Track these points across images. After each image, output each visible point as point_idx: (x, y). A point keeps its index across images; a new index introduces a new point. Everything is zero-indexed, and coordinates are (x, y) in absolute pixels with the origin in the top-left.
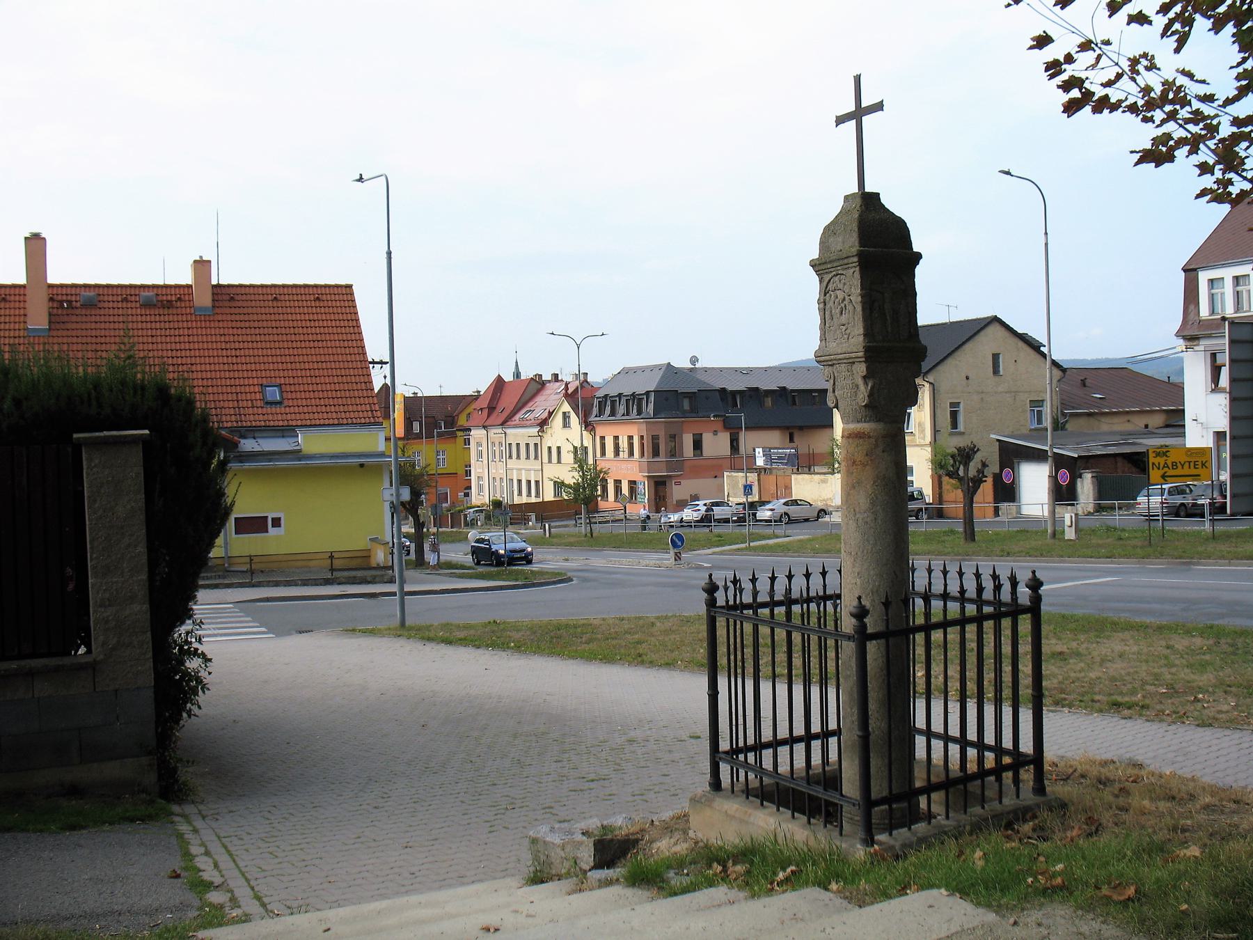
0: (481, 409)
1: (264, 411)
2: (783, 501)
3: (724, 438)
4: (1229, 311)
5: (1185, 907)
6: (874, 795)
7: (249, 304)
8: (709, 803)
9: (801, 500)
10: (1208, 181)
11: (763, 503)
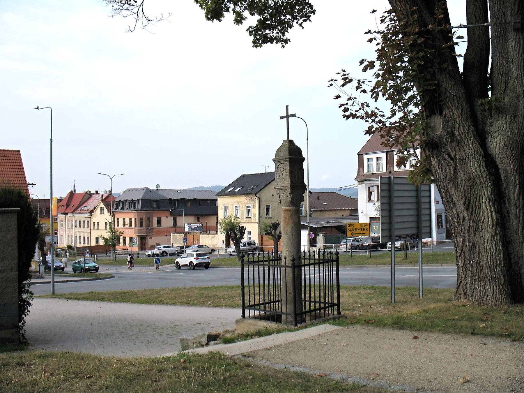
0: (63, 206)
2: (197, 245)
3: (170, 219)
4: (375, 171)
5: (386, 322)
6: (297, 312)
8: (243, 321)
9: (204, 245)
10: (383, 140)
11: (188, 247)
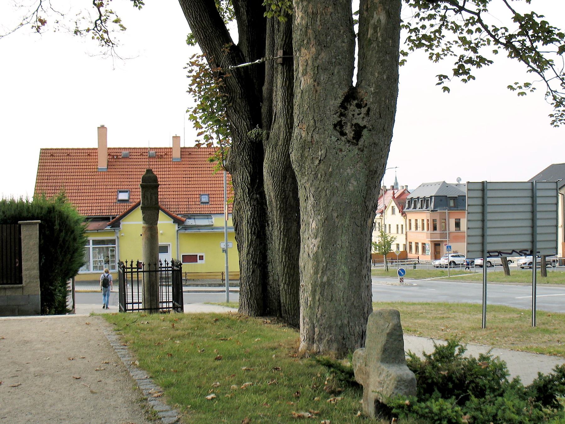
1: (200, 206)
7: (198, 156)
